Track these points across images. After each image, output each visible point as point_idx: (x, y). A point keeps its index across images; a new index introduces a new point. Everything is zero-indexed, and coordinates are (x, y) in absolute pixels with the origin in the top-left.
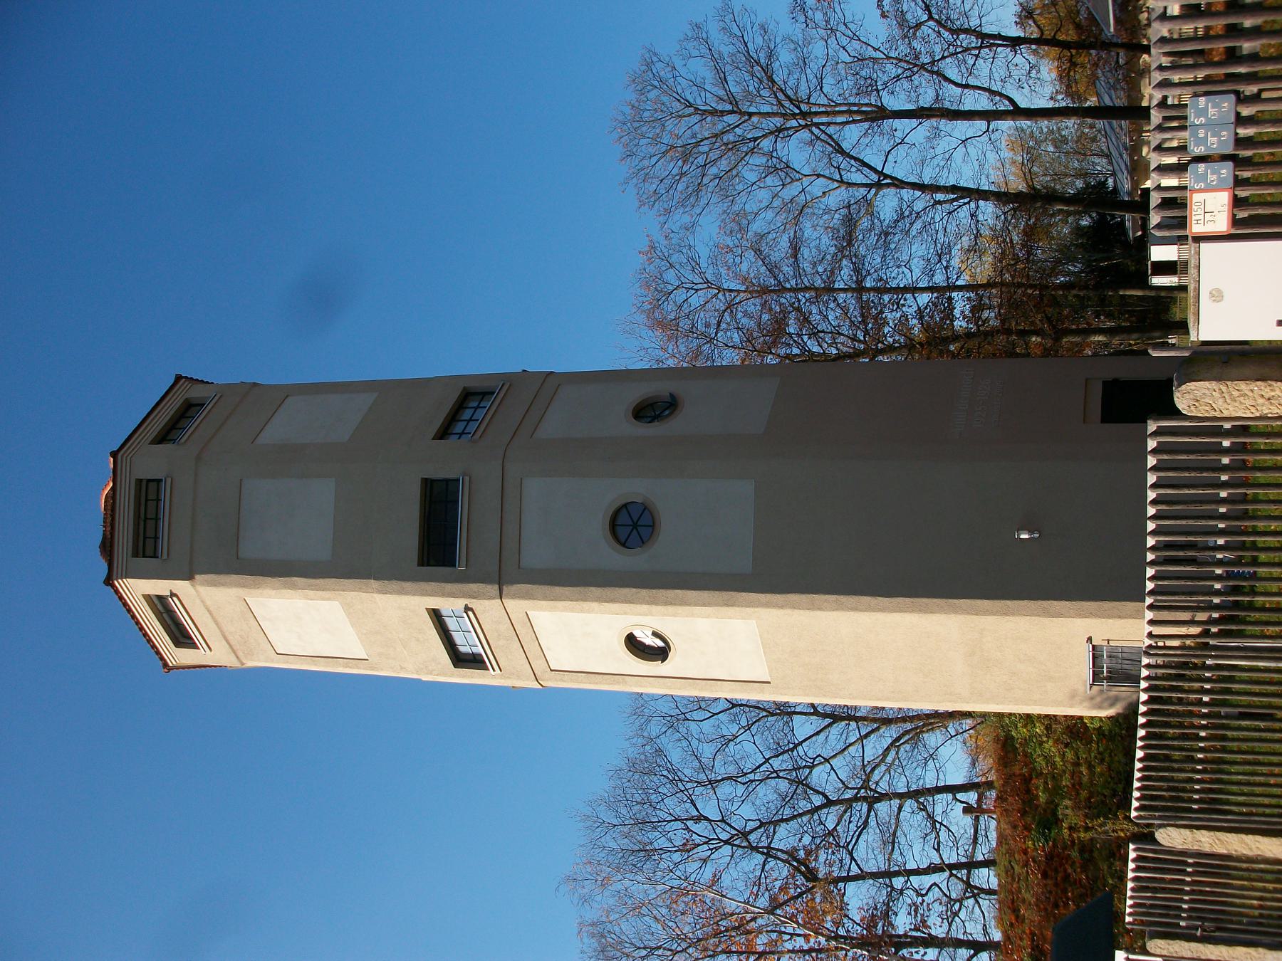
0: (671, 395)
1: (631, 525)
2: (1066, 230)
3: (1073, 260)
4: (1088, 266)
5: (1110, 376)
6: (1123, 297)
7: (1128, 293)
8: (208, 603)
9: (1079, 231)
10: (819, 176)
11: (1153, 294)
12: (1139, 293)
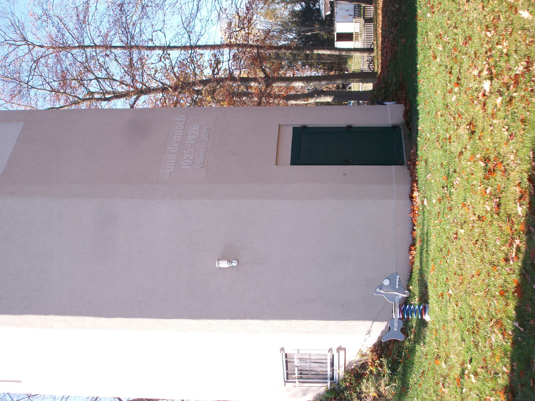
2: (286, 13)
3: (291, 31)
4: (299, 35)
5: (299, 122)
6: (319, 54)
7: (321, 52)
9: (293, 13)
11: (337, 53)
12: (327, 52)
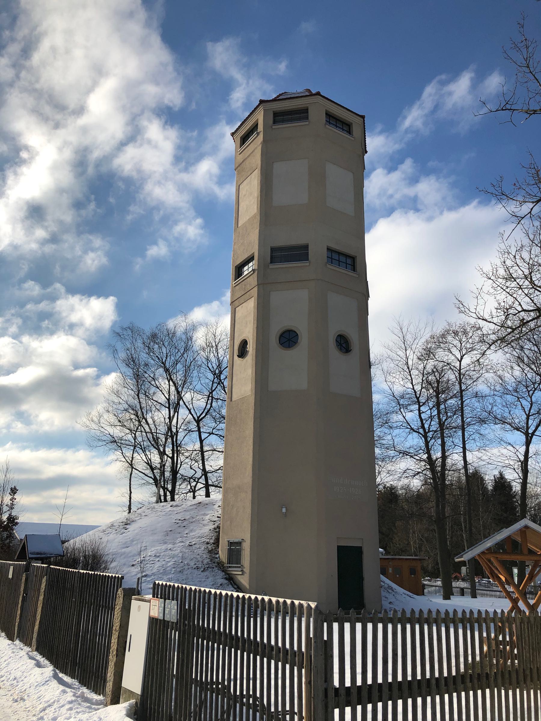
0: (350, 351)
1: (289, 339)
5: (365, 550)
8: (256, 151)
10: (531, 405)
